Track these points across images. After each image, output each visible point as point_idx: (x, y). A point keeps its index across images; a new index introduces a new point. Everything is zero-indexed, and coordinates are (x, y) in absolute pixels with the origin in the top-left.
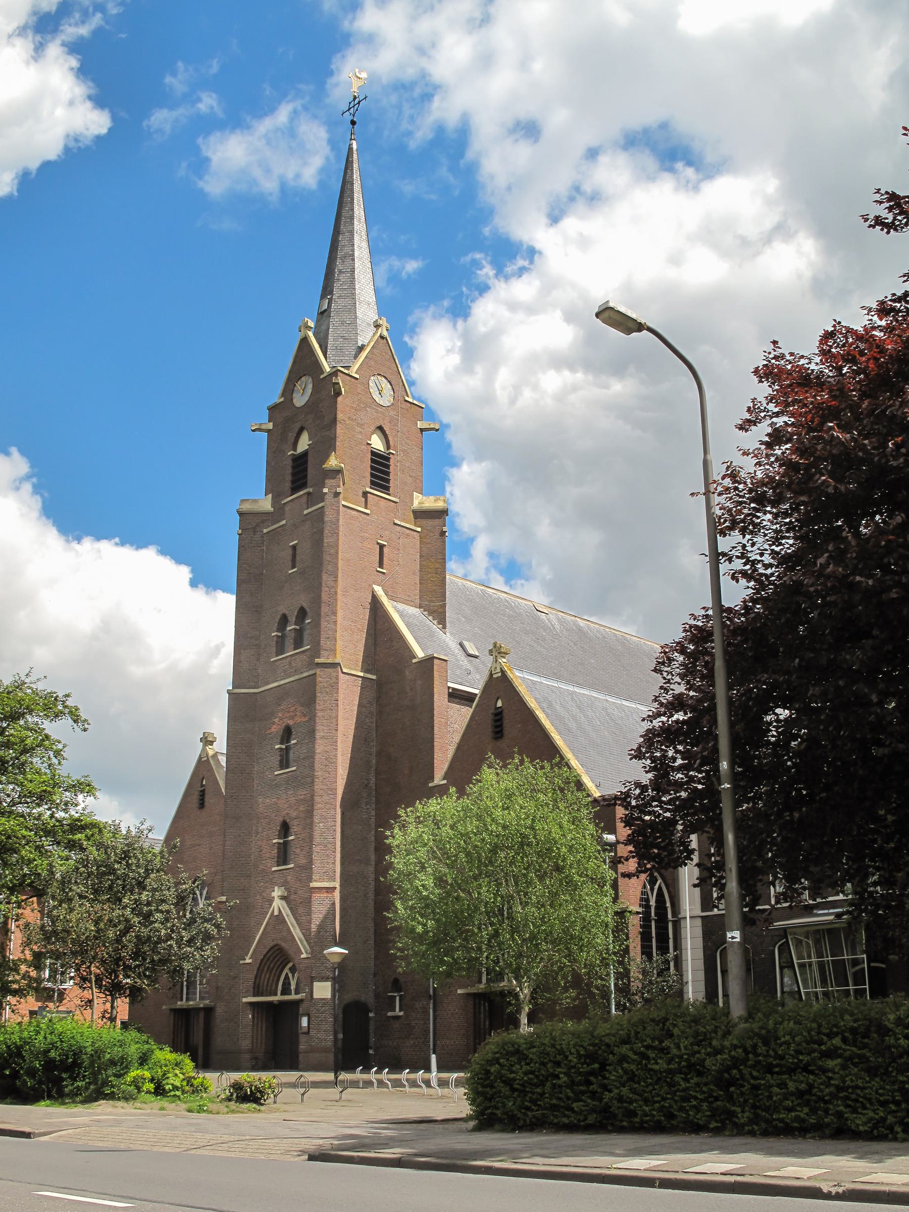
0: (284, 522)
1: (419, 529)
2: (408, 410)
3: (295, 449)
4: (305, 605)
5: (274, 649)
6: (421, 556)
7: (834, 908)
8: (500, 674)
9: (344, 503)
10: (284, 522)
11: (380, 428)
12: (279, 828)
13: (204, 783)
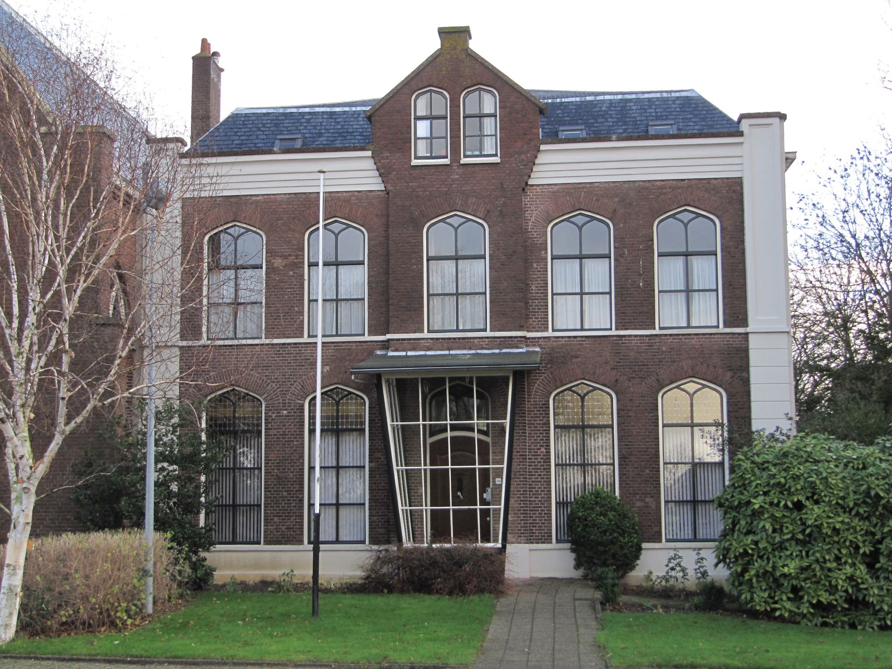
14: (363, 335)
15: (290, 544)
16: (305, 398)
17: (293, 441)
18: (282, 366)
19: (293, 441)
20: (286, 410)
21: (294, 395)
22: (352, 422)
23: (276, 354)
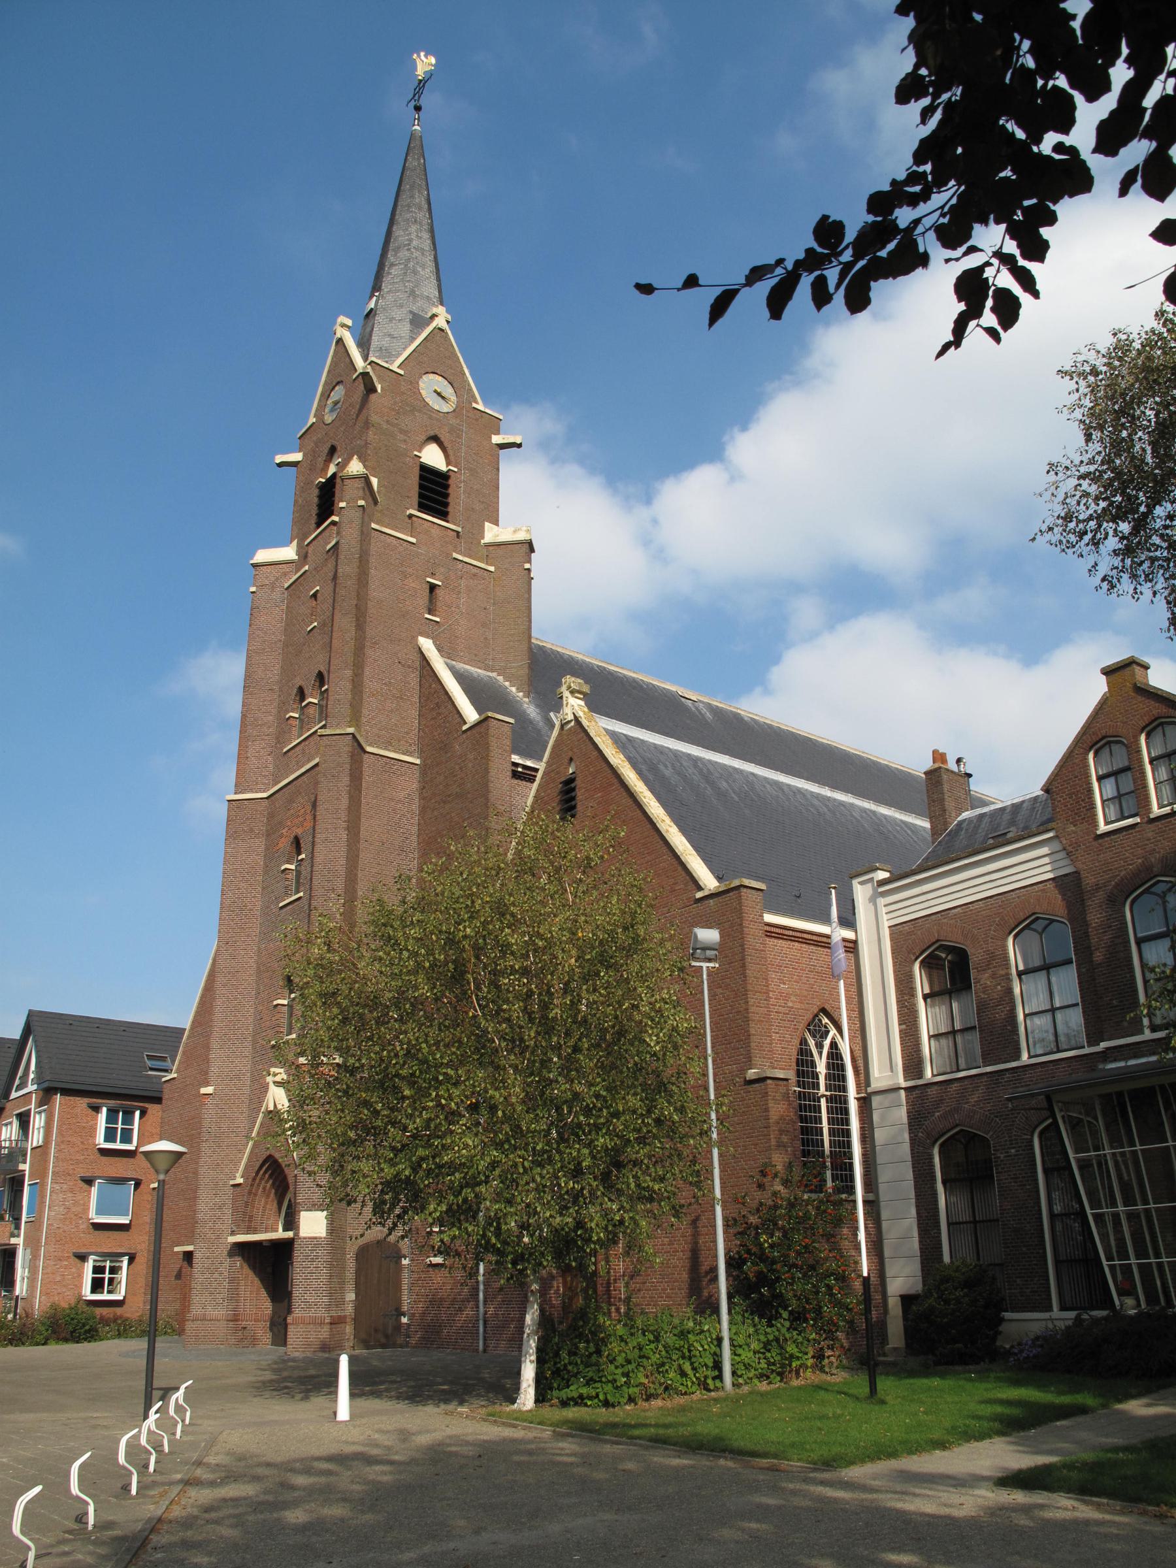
0: (307, 568)
1: (492, 569)
7: (1136, 1057)
8: (573, 724)
10: (307, 568)
15: (1037, 1311)
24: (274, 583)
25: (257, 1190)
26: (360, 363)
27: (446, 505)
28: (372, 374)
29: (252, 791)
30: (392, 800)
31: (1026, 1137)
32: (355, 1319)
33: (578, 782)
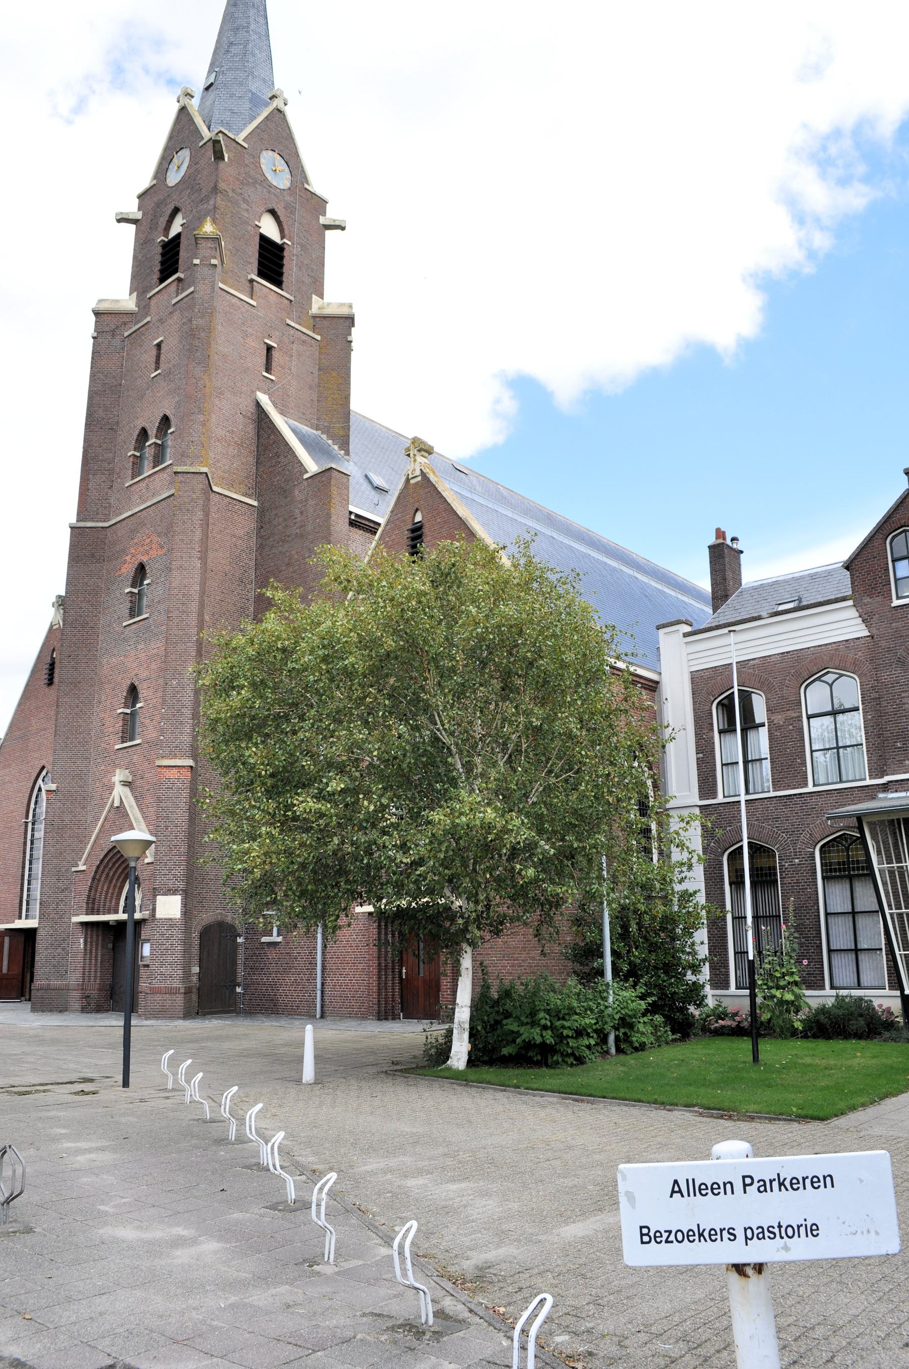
0: (148, 319)
1: (318, 338)
2: (308, 200)
3: (166, 235)
4: (168, 413)
5: (130, 472)
6: (320, 370)
8: (419, 479)
9: (221, 285)
10: (148, 319)
11: (273, 212)
12: (125, 694)
13: (54, 656)
14: (865, 779)
15: (812, 989)
16: (815, 846)
17: (806, 889)
18: (790, 817)
19: (806, 889)
20: (797, 858)
21: (804, 843)
22: (766, 874)
23: (783, 806)
24: (114, 331)
25: (100, 877)
26: (206, 134)
27: (281, 274)
28: (222, 142)
29: (92, 520)
30: (235, 536)
31: (809, 850)
32: (199, 989)
33: (425, 530)
